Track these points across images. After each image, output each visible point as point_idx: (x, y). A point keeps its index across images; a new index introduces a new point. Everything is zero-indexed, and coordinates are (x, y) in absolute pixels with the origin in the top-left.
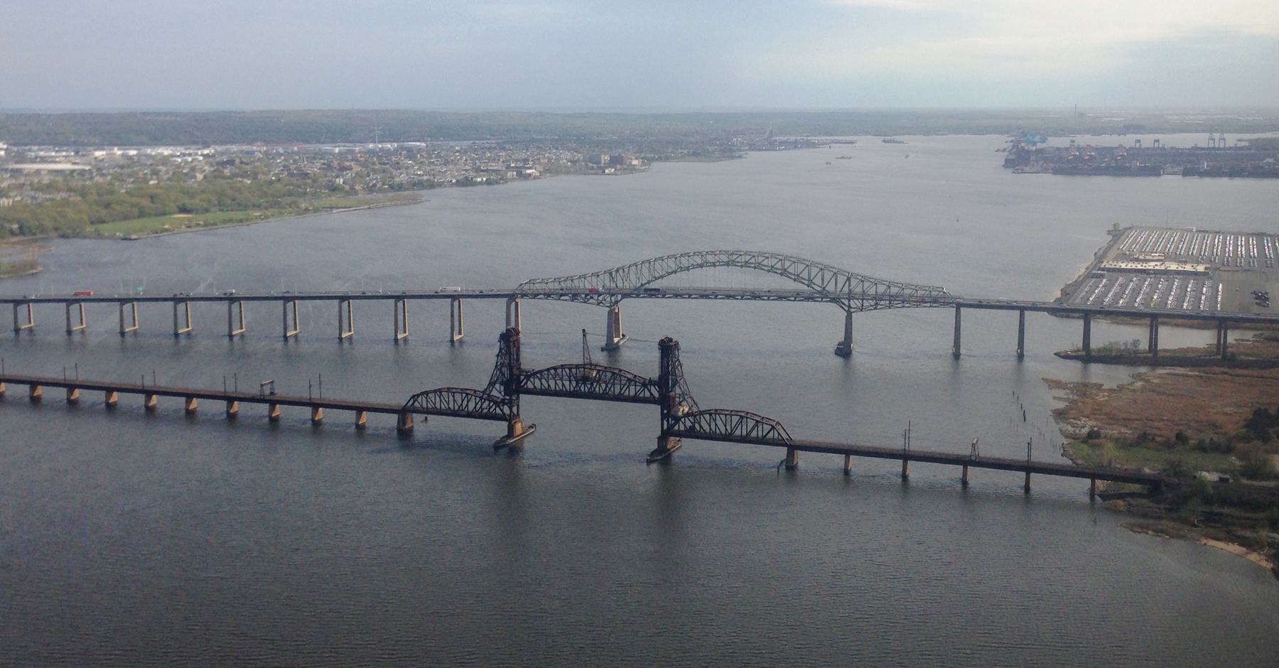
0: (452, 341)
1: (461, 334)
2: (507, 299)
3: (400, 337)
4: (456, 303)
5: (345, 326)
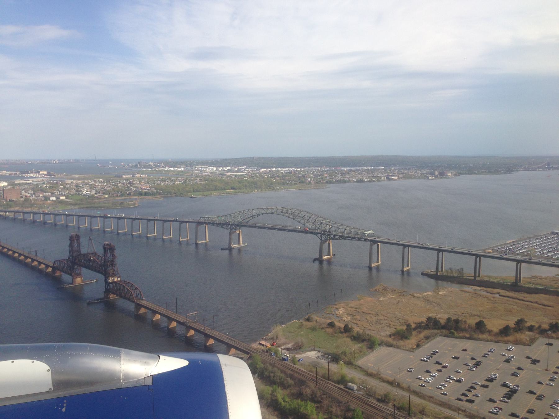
0: (403, 271)
1: (409, 267)
2: (196, 224)
3: (405, 269)
4: (478, 259)
5: (406, 264)
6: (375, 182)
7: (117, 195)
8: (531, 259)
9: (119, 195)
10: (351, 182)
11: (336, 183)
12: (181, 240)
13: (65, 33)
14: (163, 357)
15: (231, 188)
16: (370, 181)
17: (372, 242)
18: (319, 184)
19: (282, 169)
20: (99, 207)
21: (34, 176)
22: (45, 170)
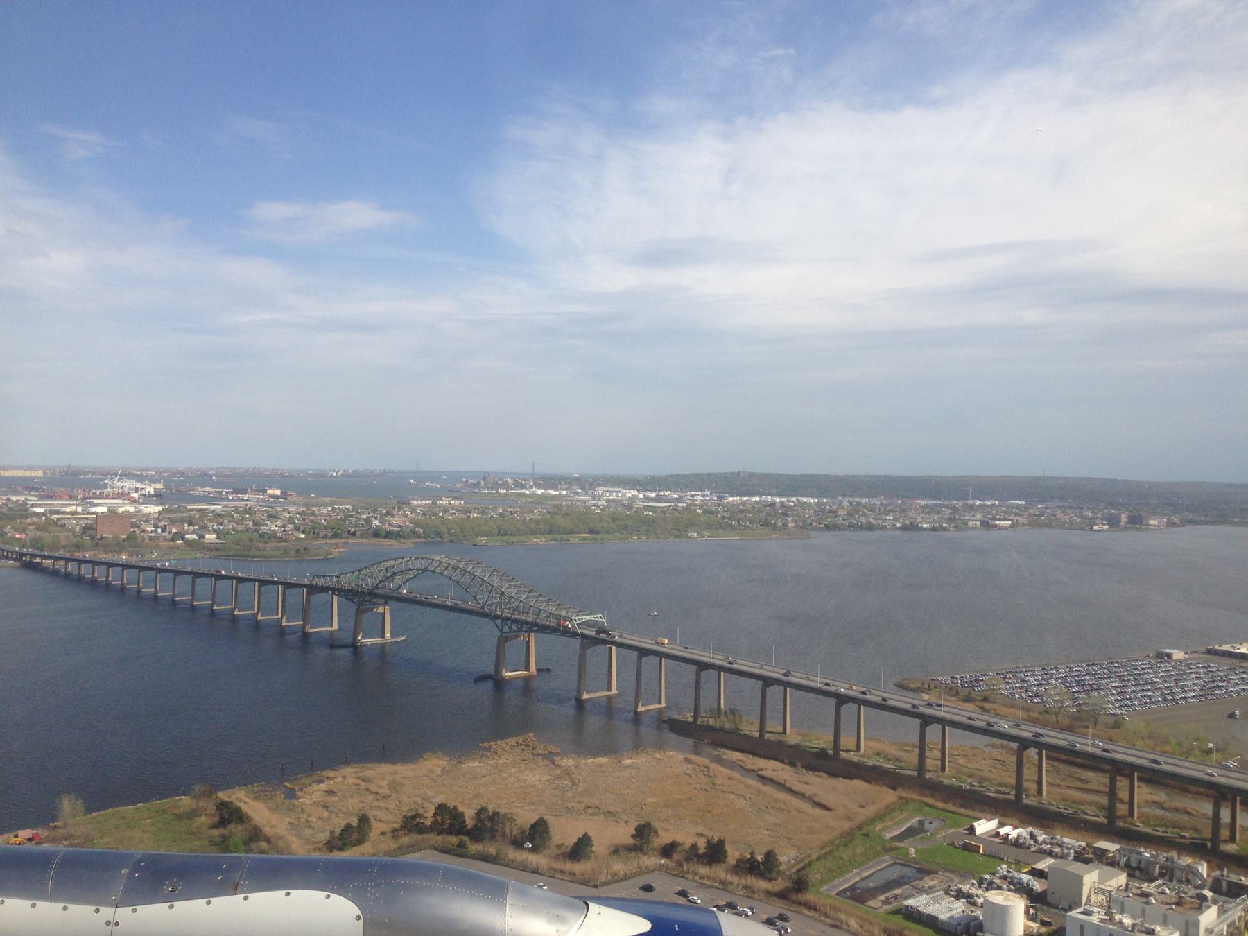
6: (949, 530)
7: (327, 536)
8: (866, 694)
9: (329, 535)
10: (887, 529)
11: (850, 530)
12: (284, 623)
13: (387, 218)
14: (597, 906)
15: (588, 530)
16: (934, 529)
17: (585, 641)
18: (807, 529)
19: (775, 499)
20: (249, 556)
21: (245, 498)
22: (278, 488)
